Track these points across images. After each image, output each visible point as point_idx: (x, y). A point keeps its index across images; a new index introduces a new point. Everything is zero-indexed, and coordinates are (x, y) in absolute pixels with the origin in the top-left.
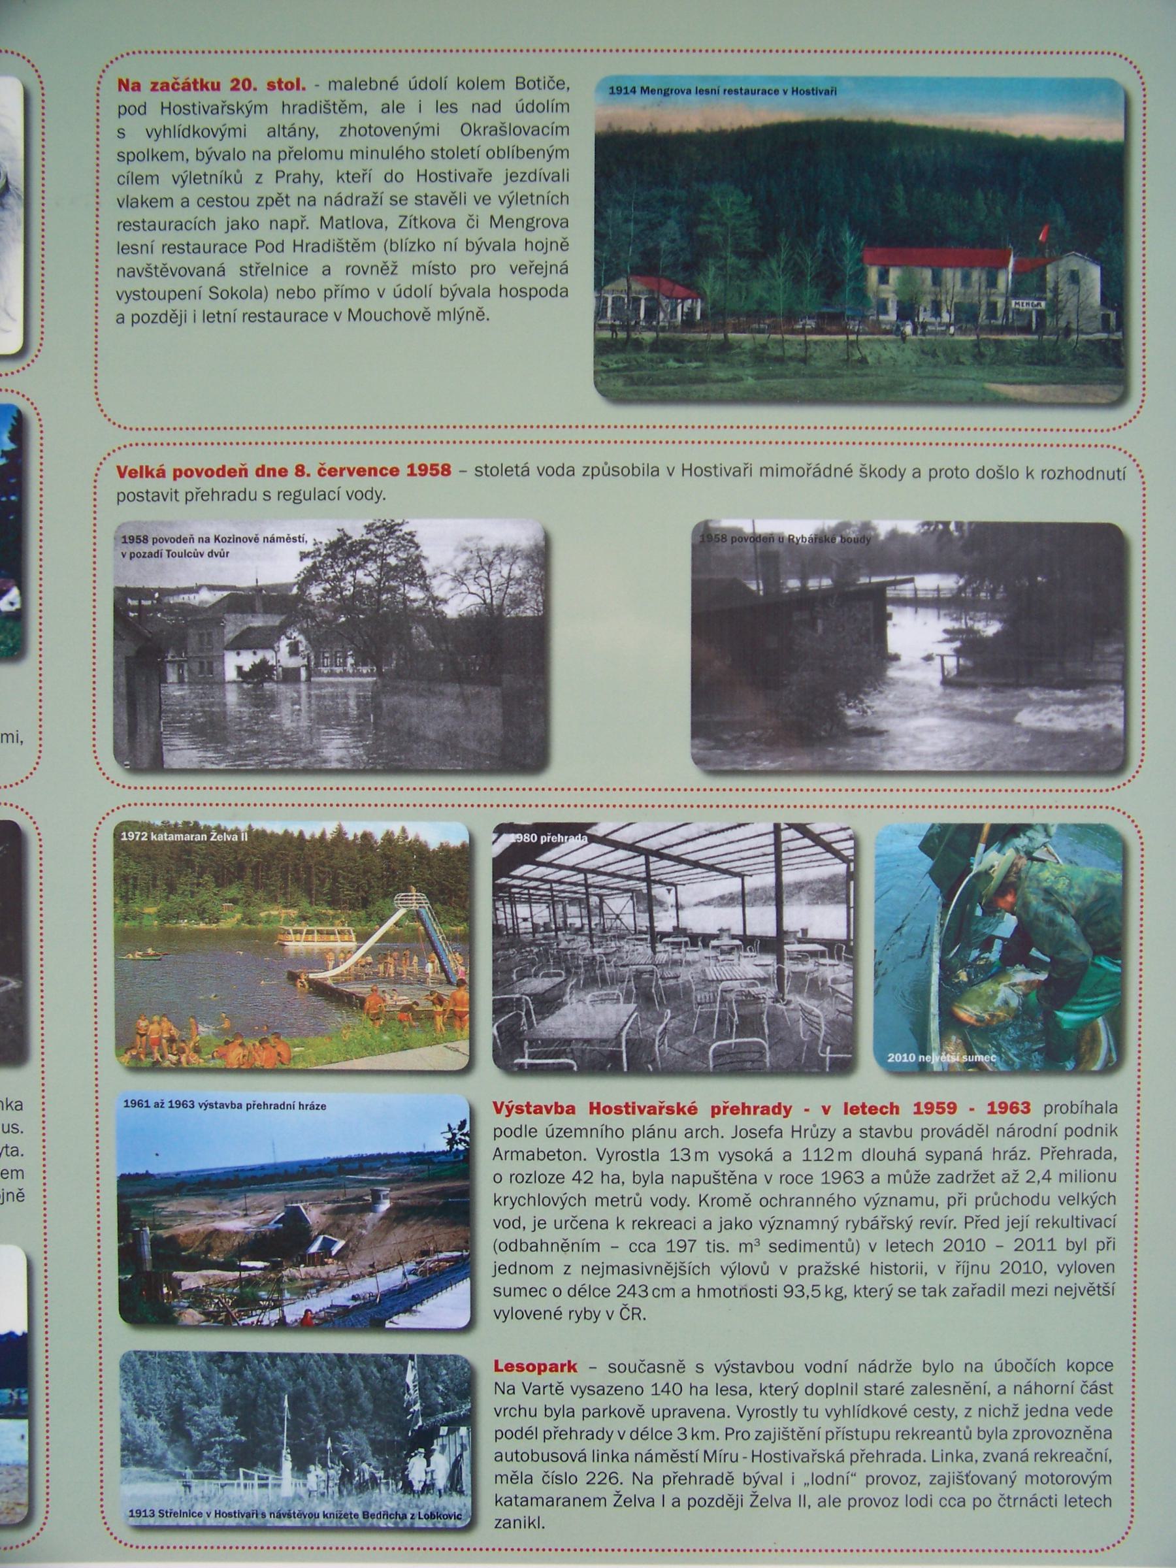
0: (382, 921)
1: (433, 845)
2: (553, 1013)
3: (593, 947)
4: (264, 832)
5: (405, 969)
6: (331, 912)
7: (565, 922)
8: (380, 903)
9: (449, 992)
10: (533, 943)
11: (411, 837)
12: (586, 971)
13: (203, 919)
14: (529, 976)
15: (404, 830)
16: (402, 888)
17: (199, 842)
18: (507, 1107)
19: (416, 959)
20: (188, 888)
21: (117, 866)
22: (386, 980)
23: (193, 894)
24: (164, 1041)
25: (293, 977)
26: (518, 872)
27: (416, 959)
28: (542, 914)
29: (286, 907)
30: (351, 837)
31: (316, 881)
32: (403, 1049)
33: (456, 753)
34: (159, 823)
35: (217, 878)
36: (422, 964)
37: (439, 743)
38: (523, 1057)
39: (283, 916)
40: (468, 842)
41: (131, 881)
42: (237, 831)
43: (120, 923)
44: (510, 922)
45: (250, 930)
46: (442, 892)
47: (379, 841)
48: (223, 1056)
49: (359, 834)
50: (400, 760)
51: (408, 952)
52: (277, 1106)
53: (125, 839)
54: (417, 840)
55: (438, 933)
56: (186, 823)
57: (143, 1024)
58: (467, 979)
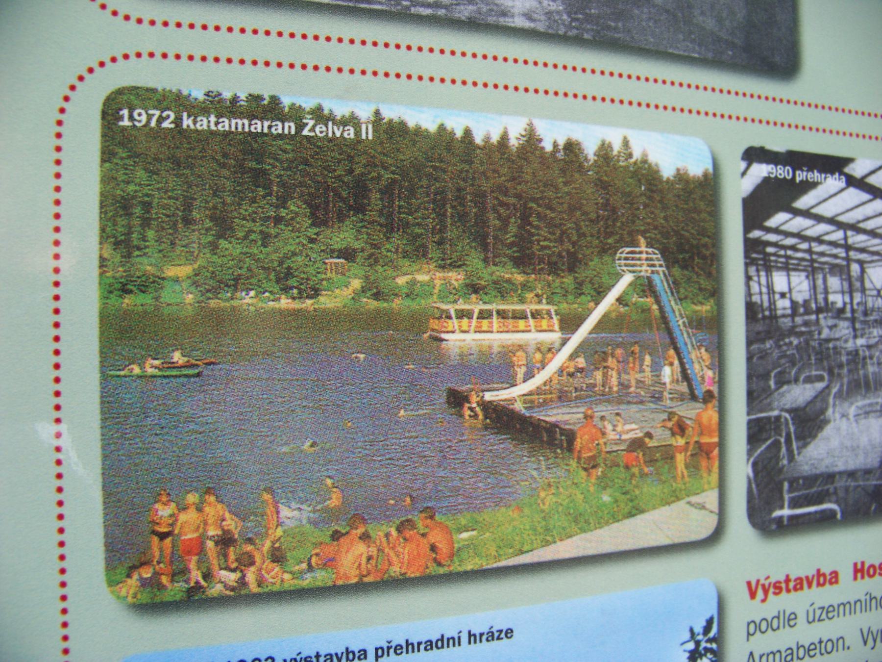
0: (600, 294)
1: (667, 172)
2: (815, 436)
3: (855, 337)
4: (403, 124)
5: (633, 377)
6: (519, 278)
7: (826, 299)
8: (595, 263)
9: (692, 414)
10: (792, 331)
11: (637, 155)
12: (850, 371)
13: (286, 290)
14: (788, 382)
15: (626, 143)
16: (628, 239)
17: (281, 136)
18: (763, 586)
19: (648, 359)
20: (257, 227)
21: (107, 179)
22: (606, 397)
23: (266, 238)
24: (210, 544)
25: (457, 399)
26: (772, 222)
27: (648, 359)
28: (800, 286)
29: (443, 267)
30: (548, 147)
31: (494, 222)
32: (630, 515)
33: (691, 33)
34: (199, 94)
35: (314, 209)
36: (656, 368)
37: (667, 11)
38: (782, 507)
39: (438, 283)
40: (711, 170)
41: (138, 211)
42: (352, 121)
43: (113, 300)
44: (765, 298)
45: (378, 311)
46: (681, 250)
47: (592, 157)
48: (329, 563)
49: (561, 142)
50: (616, 29)
51: (637, 349)
52: (430, 645)
53: (126, 123)
54: (645, 161)
55: (678, 313)
56: (255, 99)
57: (164, 511)
58: (715, 389)
